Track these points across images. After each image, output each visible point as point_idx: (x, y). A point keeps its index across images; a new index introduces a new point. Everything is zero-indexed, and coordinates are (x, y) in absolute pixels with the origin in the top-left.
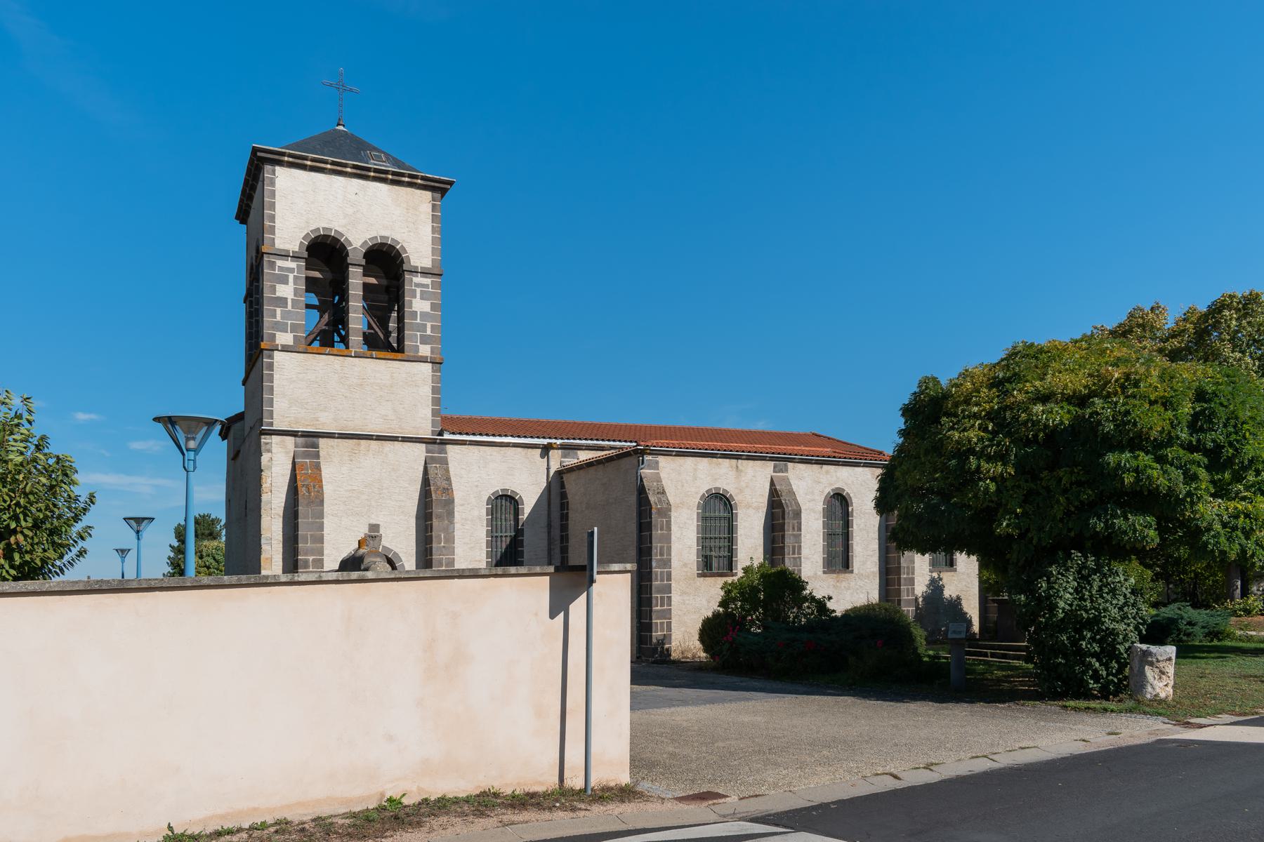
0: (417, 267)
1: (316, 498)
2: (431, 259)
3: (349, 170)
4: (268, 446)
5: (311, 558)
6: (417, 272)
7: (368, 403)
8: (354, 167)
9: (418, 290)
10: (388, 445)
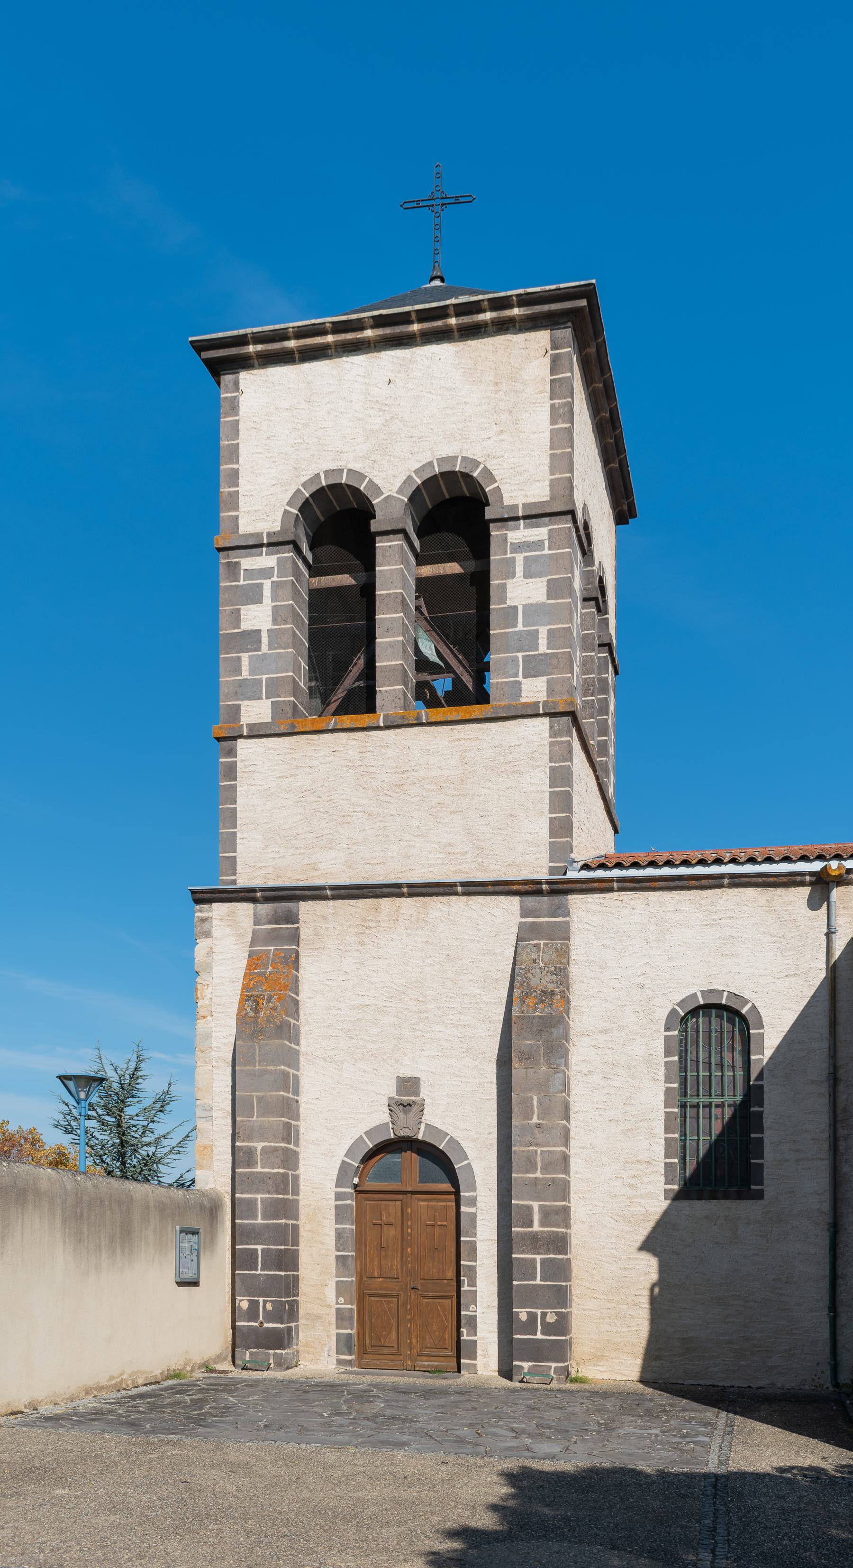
0: (516, 506)
1: (268, 1021)
2: (547, 483)
3: (369, 333)
4: (206, 925)
5: (259, 1146)
6: (517, 519)
9: (520, 558)
10: (438, 905)
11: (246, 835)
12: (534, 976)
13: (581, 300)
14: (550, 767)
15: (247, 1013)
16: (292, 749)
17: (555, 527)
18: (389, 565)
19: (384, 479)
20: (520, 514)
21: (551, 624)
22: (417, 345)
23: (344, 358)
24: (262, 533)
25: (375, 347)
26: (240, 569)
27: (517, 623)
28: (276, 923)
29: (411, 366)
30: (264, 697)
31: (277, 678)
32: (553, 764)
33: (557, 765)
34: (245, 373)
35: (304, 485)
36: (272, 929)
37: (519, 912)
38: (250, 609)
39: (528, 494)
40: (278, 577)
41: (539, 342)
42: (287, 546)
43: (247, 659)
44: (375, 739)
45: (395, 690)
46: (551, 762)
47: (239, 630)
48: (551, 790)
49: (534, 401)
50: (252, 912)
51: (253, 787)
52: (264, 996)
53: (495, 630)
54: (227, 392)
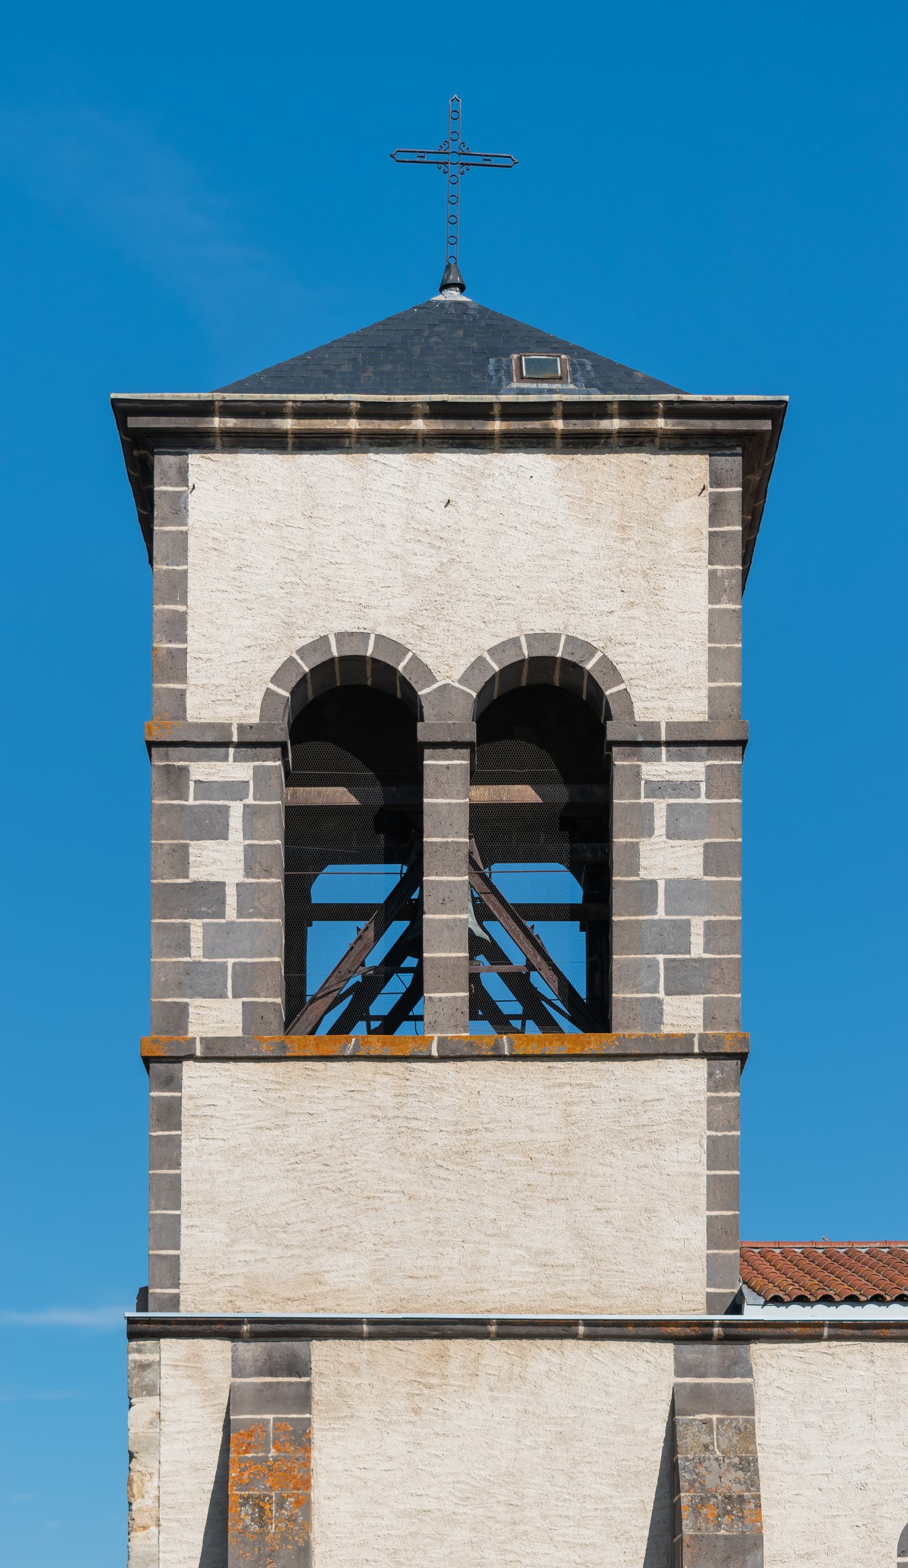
0: (656, 725)
1: (284, 1539)
2: (704, 692)
3: (419, 424)
4: (149, 1376)
6: (658, 744)
7: (489, 1214)
8: (437, 411)
9: (660, 806)
11: (196, 1221)
12: (709, 1472)
13: (763, 421)
14: (709, 1137)
15: (246, 1527)
16: (279, 1083)
17: (717, 762)
18: (445, 796)
19: (437, 657)
20: (663, 738)
21: (711, 915)
22: (493, 450)
23: (371, 455)
24: (230, 725)
25: (424, 443)
26: (188, 779)
27: (656, 907)
28: (272, 1374)
29: (484, 483)
30: (230, 994)
31: (253, 964)
32: (713, 1133)
33: (720, 1134)
34: (199, 456)
35: (300, 652)
36: (264, 1384)
37: (673, 1368)
38: (206, 848)
39: (674, 707)
40: (255, 799)
41: (691, 472)
42: (271, 750)
43: (200, 930)
44: (421, 1074)
45: (455, 998)
46: (709, 1129)
47: (187, 881)
48: (710, 1173)
49: (683, 563)
50: (229, 1355)
51: (210, 1142)
52: (271, 1497)
53: (620, 915)
54: (165, 484)
